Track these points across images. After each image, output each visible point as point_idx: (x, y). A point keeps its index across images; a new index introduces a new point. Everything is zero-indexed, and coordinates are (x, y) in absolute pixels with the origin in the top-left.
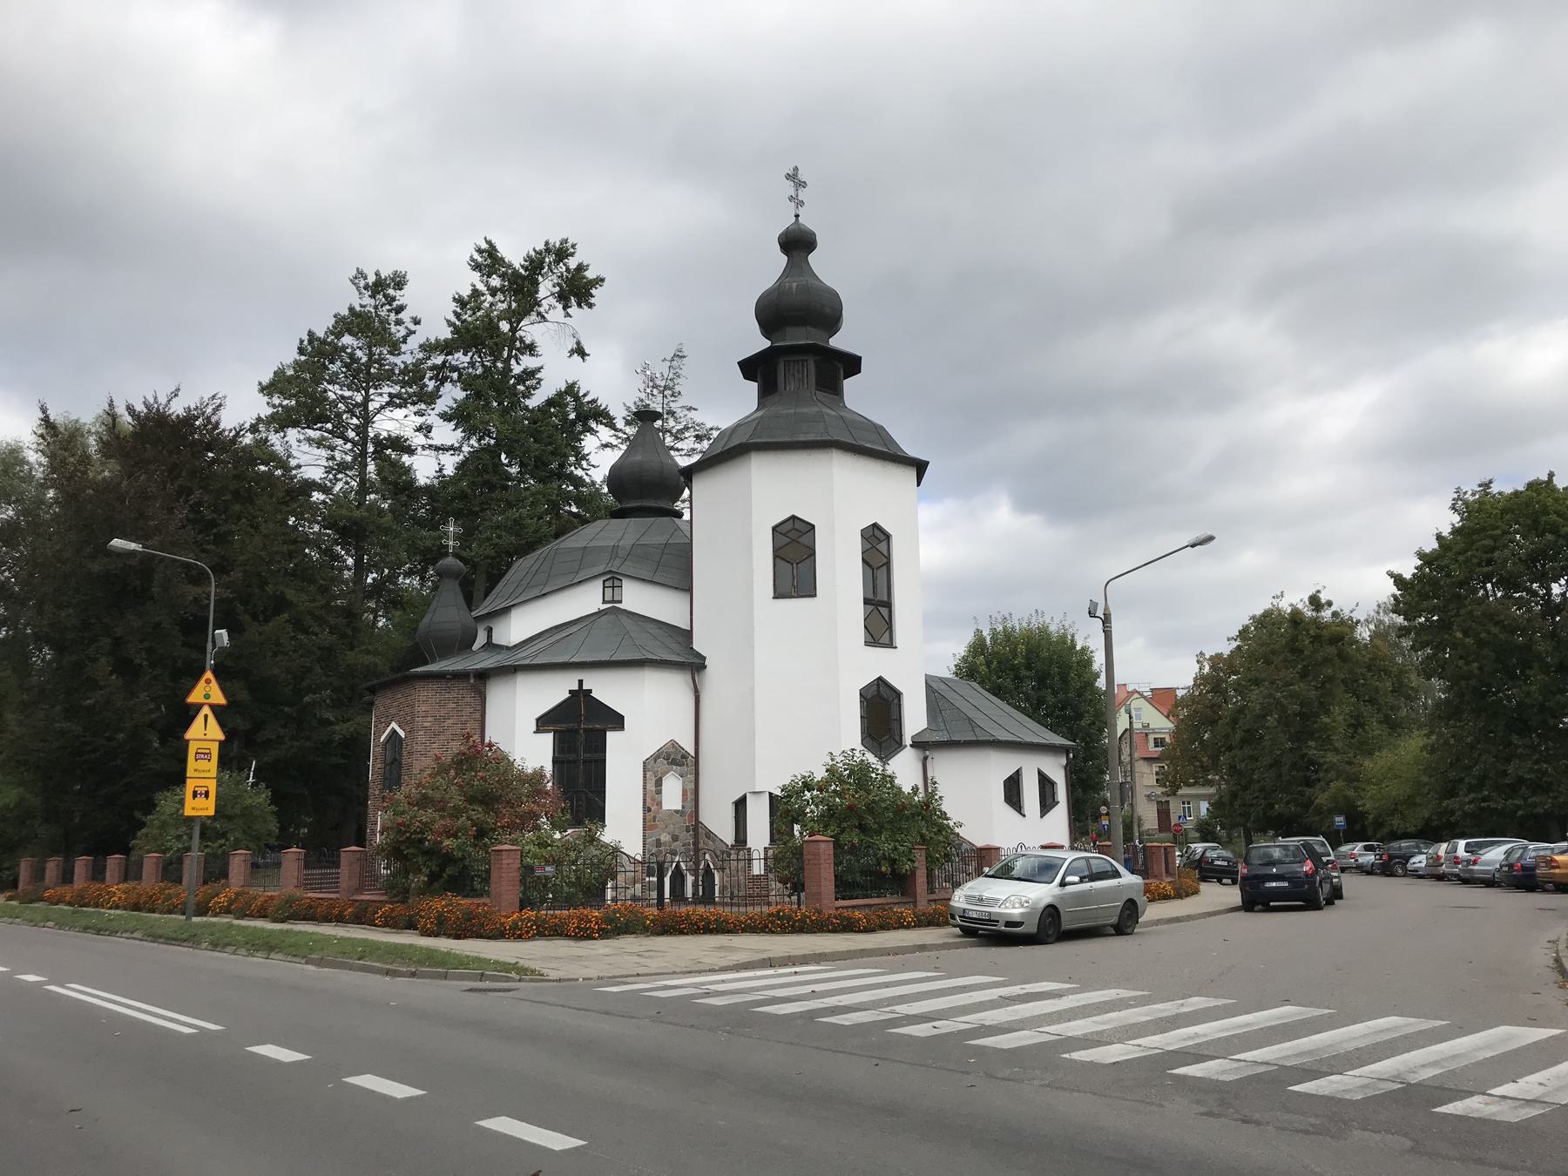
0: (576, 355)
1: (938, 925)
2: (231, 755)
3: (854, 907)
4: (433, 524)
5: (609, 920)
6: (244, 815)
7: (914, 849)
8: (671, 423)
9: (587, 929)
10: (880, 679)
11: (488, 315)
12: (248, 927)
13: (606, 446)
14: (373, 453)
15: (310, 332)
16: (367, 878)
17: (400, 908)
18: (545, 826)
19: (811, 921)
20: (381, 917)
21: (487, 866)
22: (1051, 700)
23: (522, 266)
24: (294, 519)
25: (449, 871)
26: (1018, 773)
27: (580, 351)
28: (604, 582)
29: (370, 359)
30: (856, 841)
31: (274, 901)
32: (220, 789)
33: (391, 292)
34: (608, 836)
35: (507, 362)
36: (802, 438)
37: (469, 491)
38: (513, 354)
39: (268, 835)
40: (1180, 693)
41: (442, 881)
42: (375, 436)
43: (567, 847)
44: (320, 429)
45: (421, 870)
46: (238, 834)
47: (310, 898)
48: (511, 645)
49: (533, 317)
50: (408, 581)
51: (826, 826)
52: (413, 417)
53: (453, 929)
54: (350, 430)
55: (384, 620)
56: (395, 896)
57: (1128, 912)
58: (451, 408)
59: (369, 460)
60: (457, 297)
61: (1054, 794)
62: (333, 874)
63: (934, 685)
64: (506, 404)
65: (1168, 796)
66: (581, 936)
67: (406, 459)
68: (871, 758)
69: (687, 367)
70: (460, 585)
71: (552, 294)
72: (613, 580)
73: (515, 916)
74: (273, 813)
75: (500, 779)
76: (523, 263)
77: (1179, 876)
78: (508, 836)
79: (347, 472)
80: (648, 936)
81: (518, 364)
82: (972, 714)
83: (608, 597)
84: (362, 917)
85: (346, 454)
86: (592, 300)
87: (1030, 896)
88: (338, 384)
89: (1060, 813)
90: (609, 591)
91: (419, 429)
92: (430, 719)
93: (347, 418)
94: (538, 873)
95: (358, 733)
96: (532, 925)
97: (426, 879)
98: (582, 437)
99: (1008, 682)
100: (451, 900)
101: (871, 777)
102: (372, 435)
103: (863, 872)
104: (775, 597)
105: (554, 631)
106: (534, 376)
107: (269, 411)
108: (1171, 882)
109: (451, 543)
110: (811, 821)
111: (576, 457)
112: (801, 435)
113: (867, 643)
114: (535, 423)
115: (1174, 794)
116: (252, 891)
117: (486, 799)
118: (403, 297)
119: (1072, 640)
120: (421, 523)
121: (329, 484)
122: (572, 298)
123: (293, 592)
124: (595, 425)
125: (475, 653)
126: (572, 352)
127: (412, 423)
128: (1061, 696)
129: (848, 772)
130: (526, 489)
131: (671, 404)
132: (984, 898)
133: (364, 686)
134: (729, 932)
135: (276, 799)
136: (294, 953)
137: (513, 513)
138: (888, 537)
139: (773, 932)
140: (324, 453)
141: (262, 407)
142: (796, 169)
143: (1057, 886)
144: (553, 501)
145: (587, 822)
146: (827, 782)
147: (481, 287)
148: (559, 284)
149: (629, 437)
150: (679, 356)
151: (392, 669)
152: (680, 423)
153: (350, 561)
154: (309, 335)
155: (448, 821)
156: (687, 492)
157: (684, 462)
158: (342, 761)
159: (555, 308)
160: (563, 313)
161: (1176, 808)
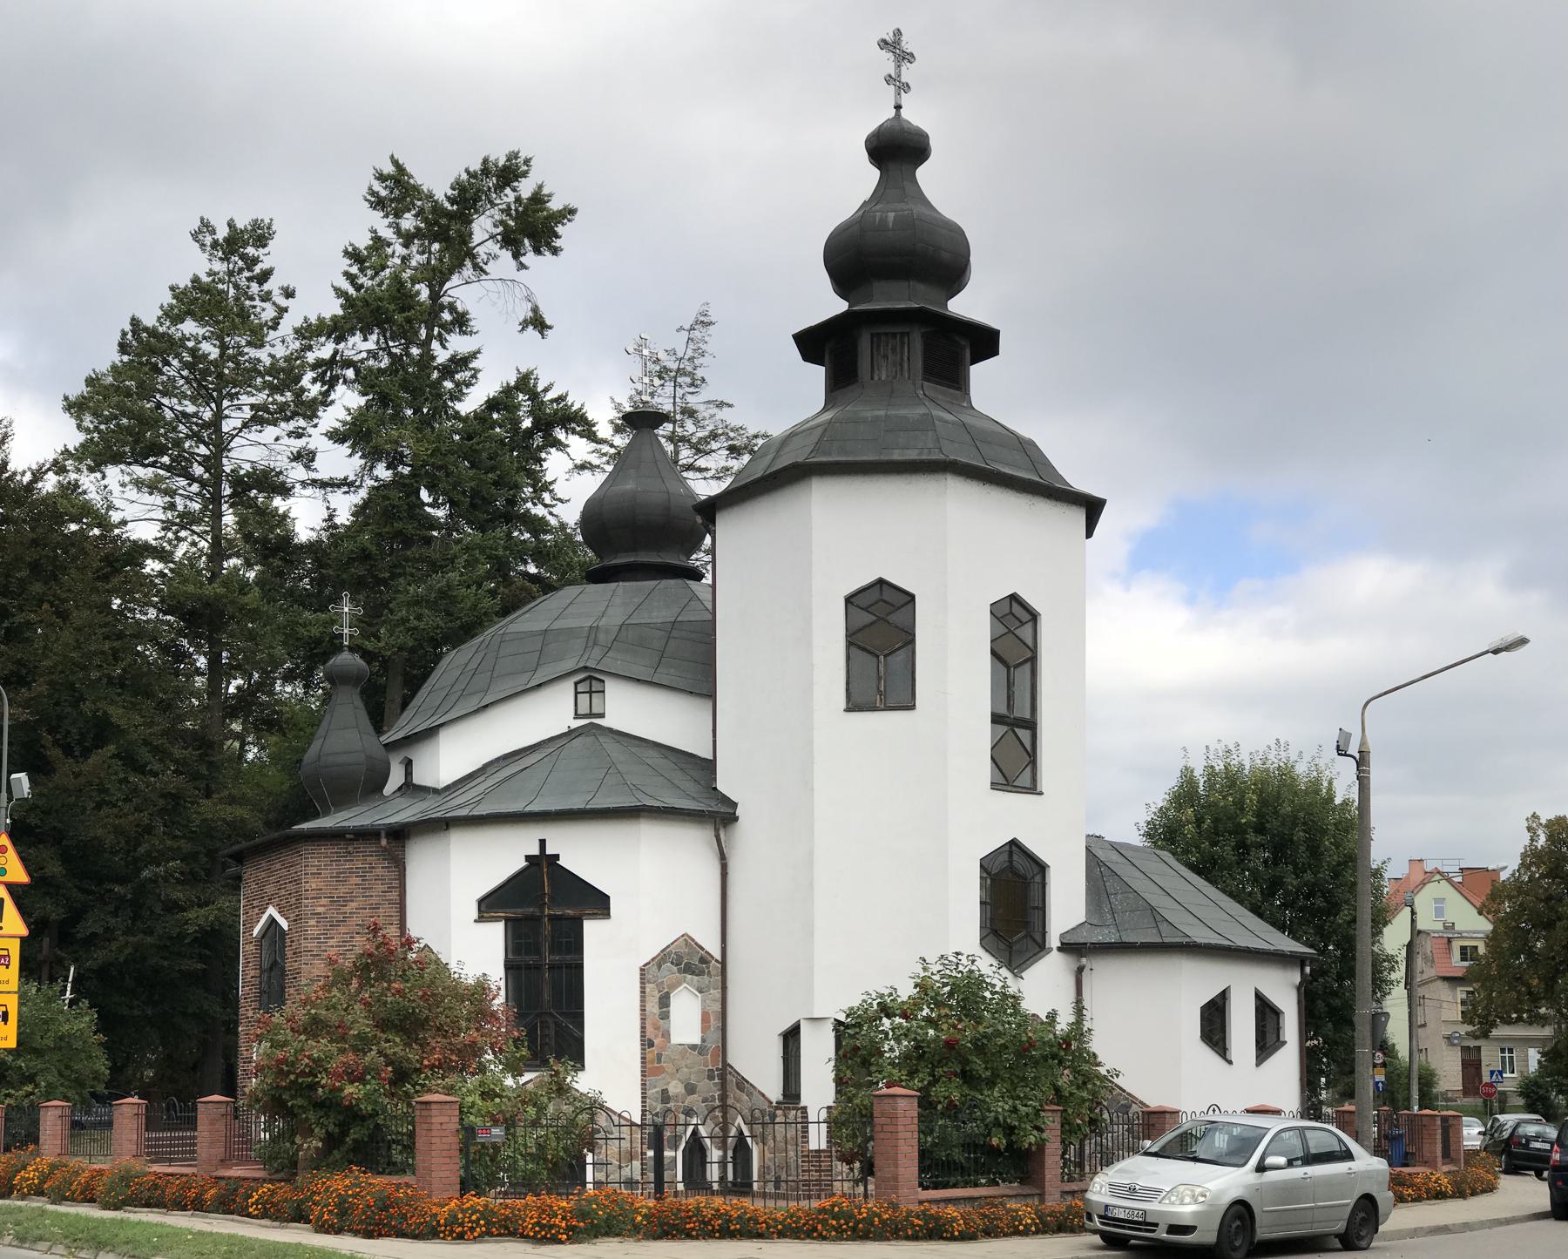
0: (531, 328)
1: (1072, 1230)
2: (40, 957)
3: (948, 1201)
4: (321, 601)
5: (583, 1215)
6: (60, 1049)
7: (1044, 1111)
8: (690, 427)
9: (551, 1227)
10: (1014, 844)
11: (396, 278)
12: (67, 1215)
13: (583, 467)
14: (230, 496)
15: (133, 319)
16: (240, 1146)
17: (284, 1190)
18: (492, 1067)
19: (882, 1222)
20: (256, 1203)
21: (410, 1127)
22: (1291, 881)
23: (448, 198)
24: (118, 601)
25: (356, 1133)
26: (1224, 995)
27: (537, 322)
28: (576, 684)
29: (222, 355)
30: (956, 1096)
31: (105, 1178)
32: (25, 1009)
33: (250, 251)
34: (584, 1082)
35: (425, 345)
36: (897, 456)
37: (374, 548)
38: (436, 333)
39: (94, 1079)
40: (1504, 876)
41: (344, 1149)
42: (232, 471)
43: (526, 1098)
44: (153, 465)
45: (313, 1131)
46: (52, 1077)
47: (155, 1174)
48: (441, 785)
49: (468, 271)
50: (289, 689)
51: (912, 1074)
52: (285, 440)
53: (361, 1222)
54: (195, 465)
55: (256, 750)
56: (277, 1171)
57: (1363, 1215)
58: (345, 423)
59: (225, 507)
60: (350, 249)
61: (1278, 1029)
62: (186, 1138)
63: (1100, 854)
64: (425, 410)
65: (1476, 1038)
66: (544, 1237)
67: (278, 502)
68: (986, 965)
69: (714, 340)
70: (362, 693)
71: (492, 237)
72: (590, 681)
73: (452, 1204)
74: (101, 1044)
75: (425, 993)
76: (450, 192)
77: (1466, 1163)
78: (439, 1082)
79: (194, 528)
80: (639, 1240)
81: (444, 347)
82: (1156, 899)
83: (583, 709)
84: (229, 1203)
85: (191, 500)
86: (557, 243)
87: (1210, 1186)
88: (175, 396)
89: (1287, 1060)
90: (583, 699)
91: (297, 457)
92: (324, 901)
93: (191, 446)
94: (481, 1138)
95: (221, 923)
96: (478, 1219)
97: (320, 1145)
98: (543, 455)
99: (1226, 851)
100: (357, 1178)
101: (985, 998)
102: (228, 469)
103: (966, 1147)
104: (848, 710)
105: (502, 763)
106: (466, 366)
107: (81, 438)
108: (1449, 1172)
109: (346, 631)
110: (889, 1064)
111: (533, 486)
112: (897, 451)
113: (995, 786)
114: (470, 438)
115: (1485, 1035)
116: (73, 1162)
117: (407, 1024)
118: (269, 257)
119: (1330, 789)
120: (303, 600)
121: (168, 548)
122: (526, 241)
123: (121, 711)
124: (564, 434)
125: (386, 800)
126: (525, 324)
127: (286, 448)
128: (1308, 876)
129: (949, 988)
130: (459, 541)
131: (690, 398)
132: (1138, 1187)
133: (226, 851)
134: (760, 1236)
135: (106, 1022)
136: (132, 1253)
137: (438, 581)
138: (1034, 617)
139: (824, 1238)
140: (159, 500)
141: (69, 435)
142: (898, 33)
143: (1252, 1171)
144: (497, 557)
145: (551, 1060)
146: (915, 1005)
147: (387, 233)
148: (502, 222)
149: (619, 453)
150: (704, 323)
151: (268, 824)
152: (703, 427)
153: (202, 662)
154: (132, 324)
155: (351, 1056)
156: (708, 540)
157: (705, 488)
158: (199, 966)
159: (496, 257)
160: (513, 263)
161: (1490, 1058)
